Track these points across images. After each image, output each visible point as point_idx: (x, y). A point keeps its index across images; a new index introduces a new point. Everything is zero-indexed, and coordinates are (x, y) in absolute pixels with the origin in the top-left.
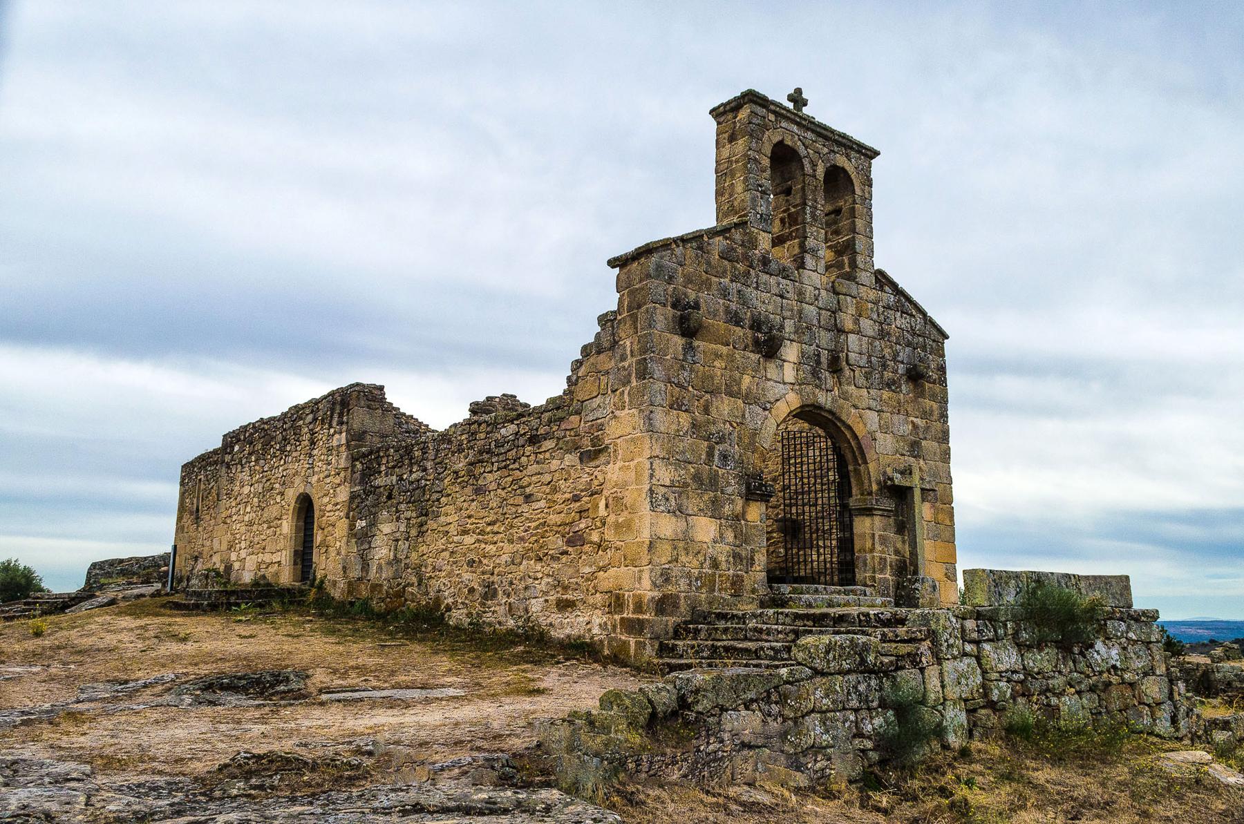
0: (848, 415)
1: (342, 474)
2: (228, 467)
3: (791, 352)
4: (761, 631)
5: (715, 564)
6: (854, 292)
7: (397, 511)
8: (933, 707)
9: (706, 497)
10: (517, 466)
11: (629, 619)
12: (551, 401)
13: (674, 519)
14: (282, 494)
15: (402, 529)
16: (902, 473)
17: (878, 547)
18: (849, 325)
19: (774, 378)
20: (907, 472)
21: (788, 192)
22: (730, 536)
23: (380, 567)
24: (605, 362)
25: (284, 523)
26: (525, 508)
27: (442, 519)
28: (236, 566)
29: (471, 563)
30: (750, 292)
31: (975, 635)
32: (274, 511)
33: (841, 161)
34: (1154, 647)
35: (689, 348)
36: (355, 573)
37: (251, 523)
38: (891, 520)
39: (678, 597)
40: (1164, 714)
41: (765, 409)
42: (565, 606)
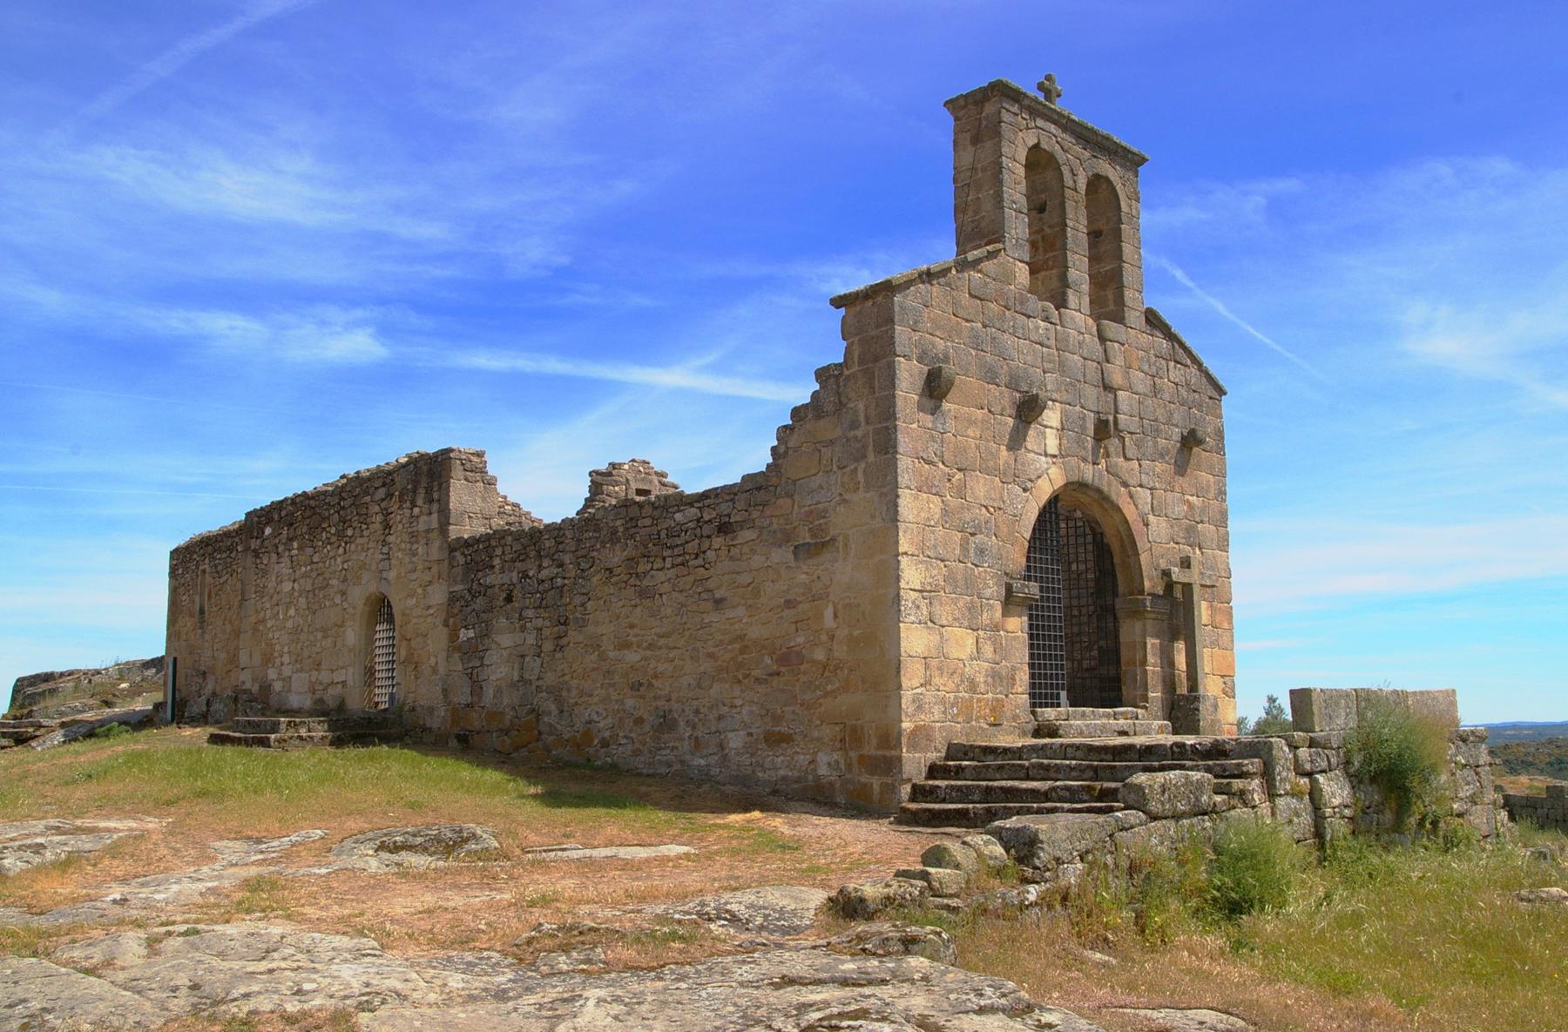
0: (1118, 495)
1: (435, 569)
2: (257, 556)
5: (973, 687)
6: (1123, 338)
9: (961, 604)
10: (700, 561)
14: (343, 593)
15: (531, 640)
19: (1035, 448)
22: (988, 650)
23: (499, 691)
24: (827, 429)
26: (713, 617)
27: (590, 629)
28: (278, 686)
29: (636, 687)
30: (1008, 340)
31: (1308, 767)
36: (462, 697)
37: (297, 631)
41: (1025, 490)
42: (776, 740)
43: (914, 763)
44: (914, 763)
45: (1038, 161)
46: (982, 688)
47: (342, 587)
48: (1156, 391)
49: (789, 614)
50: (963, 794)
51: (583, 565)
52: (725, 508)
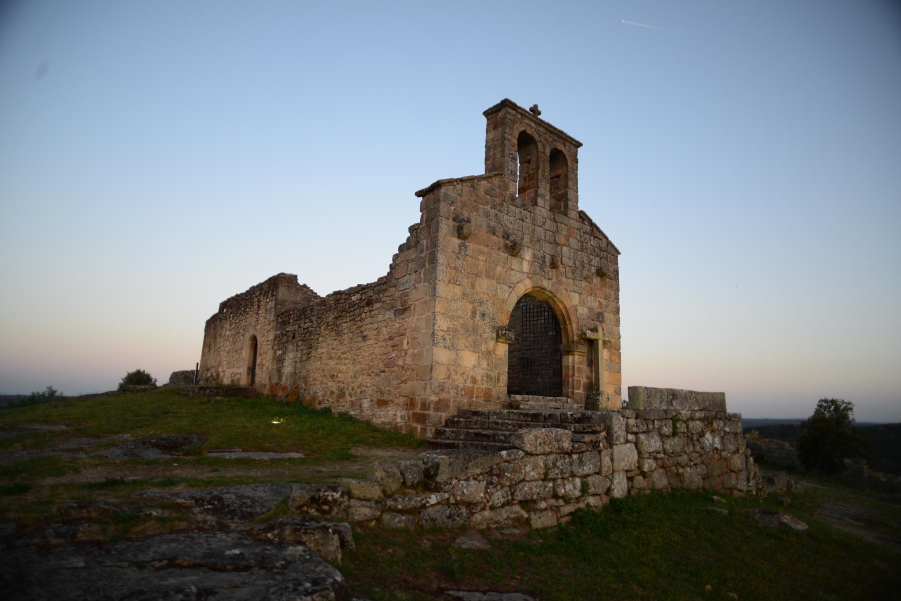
3: (528, 255)
4: (497, 424)
5: (474, 381)
6: (566, 222)
7: (297, 346)
8: (606, 477)
11: (417, 414)
12: (380, 279)
13: (448, 351)
14: (243, 335)
15: (299, 356)
16: (592, 330)
17: (576, 374)
18: (562, 240)
20: (594, 330)
21: (529, 162)
22: (484, 364)
24: (412, 254)
25: (244, 352)
27: (320, 350)
28: (221, 374)
31: (635, 429)
32: (239, 345)
33: (560, 147)
34: (739, 436)
35: (462, 246)
36: (275, 381)
38: (585, 358)
39: (449, 401)
40: (743, 475)
42: (382, 403)
49: (390, 342)
52: (371, 293)
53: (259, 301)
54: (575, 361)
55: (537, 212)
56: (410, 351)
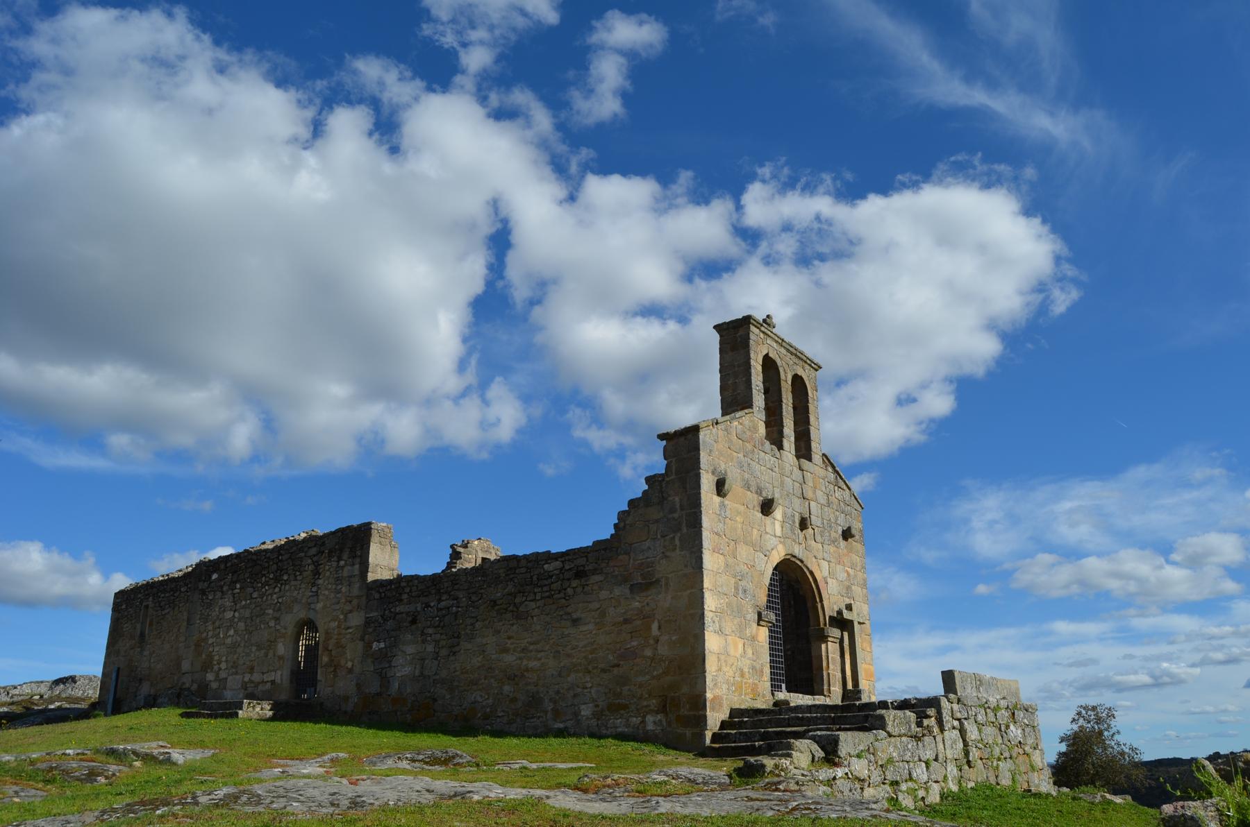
1: (355, 602)
3: (778, 513)
10: (562, 595)
14: (277, 619)
15: (430, 648)
22: (749, 652)
37: (234, 646)
43: (715, 718)
44: (715, 718)
45: (769, 365)
46: (747, 675)
47: (277, 615)
48: (829, 504)
50: (747, 737)
51: (474, 598)
52: (581, 561)
53: (317, 564)
54: (830, 650)
55: (784, 458)
56: (664, 638)
